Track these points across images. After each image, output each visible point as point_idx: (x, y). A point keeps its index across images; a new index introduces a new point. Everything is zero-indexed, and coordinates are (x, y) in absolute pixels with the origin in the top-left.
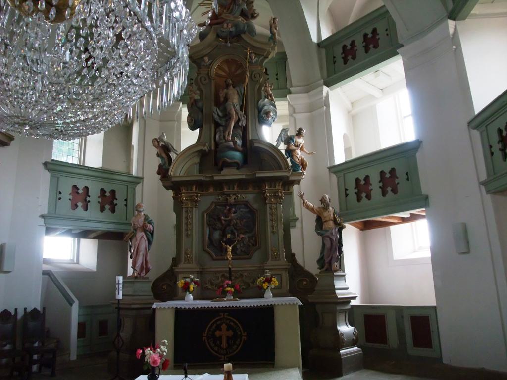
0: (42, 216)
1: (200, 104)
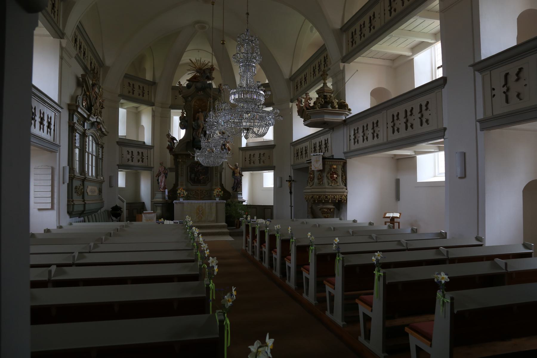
0: (118, 165)
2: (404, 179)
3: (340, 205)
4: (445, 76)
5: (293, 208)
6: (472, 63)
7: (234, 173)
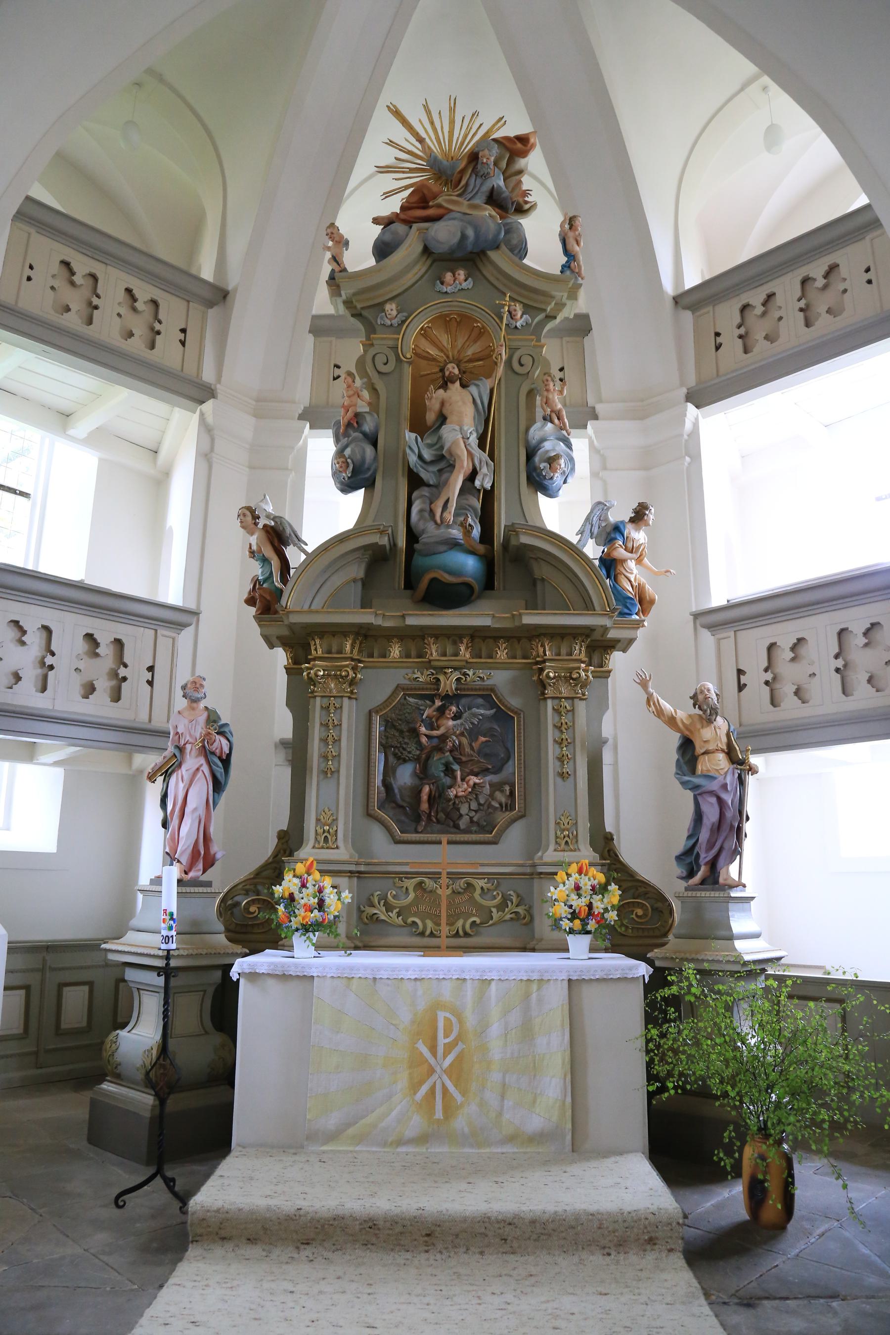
7: (688, 750)
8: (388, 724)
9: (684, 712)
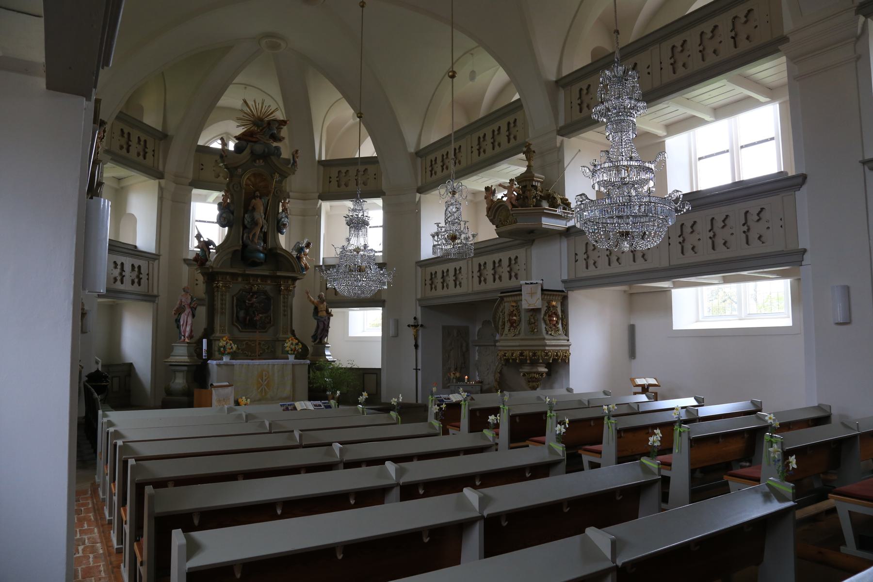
1: (232, 208)
2: (645, 326)
3: (558, 364)
4: (803, 171)
5: (420, 373)
6: (861, 159)
7: (316, 311)
8: (237, 300)
9: (316, 300)
